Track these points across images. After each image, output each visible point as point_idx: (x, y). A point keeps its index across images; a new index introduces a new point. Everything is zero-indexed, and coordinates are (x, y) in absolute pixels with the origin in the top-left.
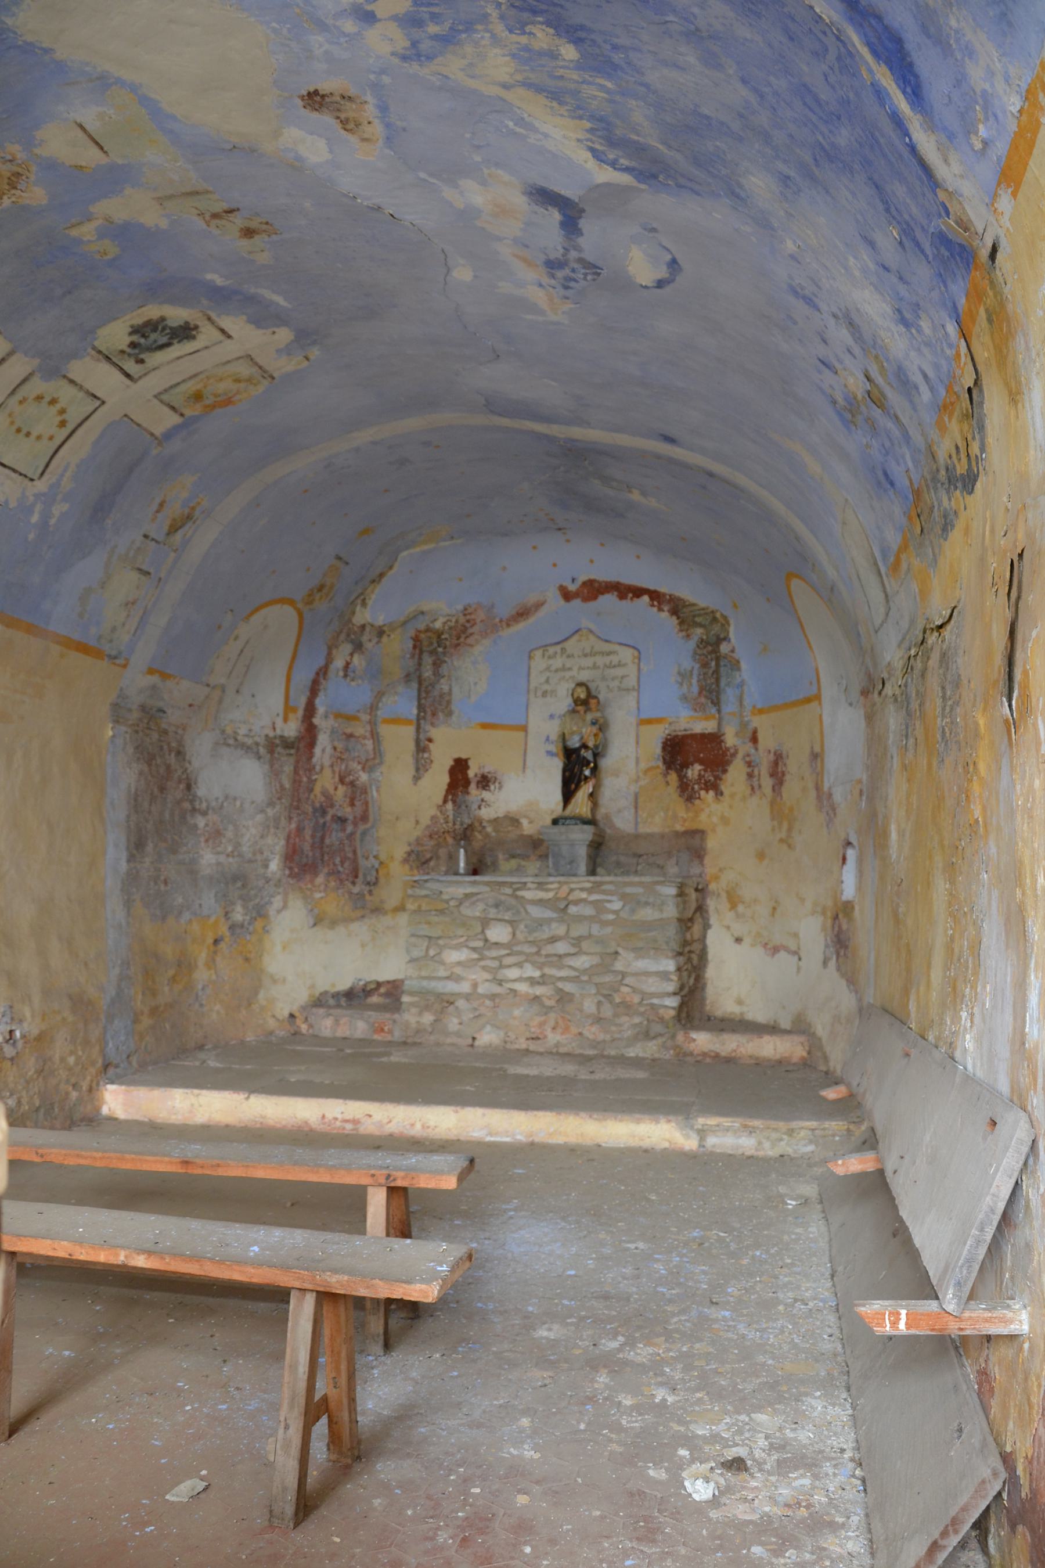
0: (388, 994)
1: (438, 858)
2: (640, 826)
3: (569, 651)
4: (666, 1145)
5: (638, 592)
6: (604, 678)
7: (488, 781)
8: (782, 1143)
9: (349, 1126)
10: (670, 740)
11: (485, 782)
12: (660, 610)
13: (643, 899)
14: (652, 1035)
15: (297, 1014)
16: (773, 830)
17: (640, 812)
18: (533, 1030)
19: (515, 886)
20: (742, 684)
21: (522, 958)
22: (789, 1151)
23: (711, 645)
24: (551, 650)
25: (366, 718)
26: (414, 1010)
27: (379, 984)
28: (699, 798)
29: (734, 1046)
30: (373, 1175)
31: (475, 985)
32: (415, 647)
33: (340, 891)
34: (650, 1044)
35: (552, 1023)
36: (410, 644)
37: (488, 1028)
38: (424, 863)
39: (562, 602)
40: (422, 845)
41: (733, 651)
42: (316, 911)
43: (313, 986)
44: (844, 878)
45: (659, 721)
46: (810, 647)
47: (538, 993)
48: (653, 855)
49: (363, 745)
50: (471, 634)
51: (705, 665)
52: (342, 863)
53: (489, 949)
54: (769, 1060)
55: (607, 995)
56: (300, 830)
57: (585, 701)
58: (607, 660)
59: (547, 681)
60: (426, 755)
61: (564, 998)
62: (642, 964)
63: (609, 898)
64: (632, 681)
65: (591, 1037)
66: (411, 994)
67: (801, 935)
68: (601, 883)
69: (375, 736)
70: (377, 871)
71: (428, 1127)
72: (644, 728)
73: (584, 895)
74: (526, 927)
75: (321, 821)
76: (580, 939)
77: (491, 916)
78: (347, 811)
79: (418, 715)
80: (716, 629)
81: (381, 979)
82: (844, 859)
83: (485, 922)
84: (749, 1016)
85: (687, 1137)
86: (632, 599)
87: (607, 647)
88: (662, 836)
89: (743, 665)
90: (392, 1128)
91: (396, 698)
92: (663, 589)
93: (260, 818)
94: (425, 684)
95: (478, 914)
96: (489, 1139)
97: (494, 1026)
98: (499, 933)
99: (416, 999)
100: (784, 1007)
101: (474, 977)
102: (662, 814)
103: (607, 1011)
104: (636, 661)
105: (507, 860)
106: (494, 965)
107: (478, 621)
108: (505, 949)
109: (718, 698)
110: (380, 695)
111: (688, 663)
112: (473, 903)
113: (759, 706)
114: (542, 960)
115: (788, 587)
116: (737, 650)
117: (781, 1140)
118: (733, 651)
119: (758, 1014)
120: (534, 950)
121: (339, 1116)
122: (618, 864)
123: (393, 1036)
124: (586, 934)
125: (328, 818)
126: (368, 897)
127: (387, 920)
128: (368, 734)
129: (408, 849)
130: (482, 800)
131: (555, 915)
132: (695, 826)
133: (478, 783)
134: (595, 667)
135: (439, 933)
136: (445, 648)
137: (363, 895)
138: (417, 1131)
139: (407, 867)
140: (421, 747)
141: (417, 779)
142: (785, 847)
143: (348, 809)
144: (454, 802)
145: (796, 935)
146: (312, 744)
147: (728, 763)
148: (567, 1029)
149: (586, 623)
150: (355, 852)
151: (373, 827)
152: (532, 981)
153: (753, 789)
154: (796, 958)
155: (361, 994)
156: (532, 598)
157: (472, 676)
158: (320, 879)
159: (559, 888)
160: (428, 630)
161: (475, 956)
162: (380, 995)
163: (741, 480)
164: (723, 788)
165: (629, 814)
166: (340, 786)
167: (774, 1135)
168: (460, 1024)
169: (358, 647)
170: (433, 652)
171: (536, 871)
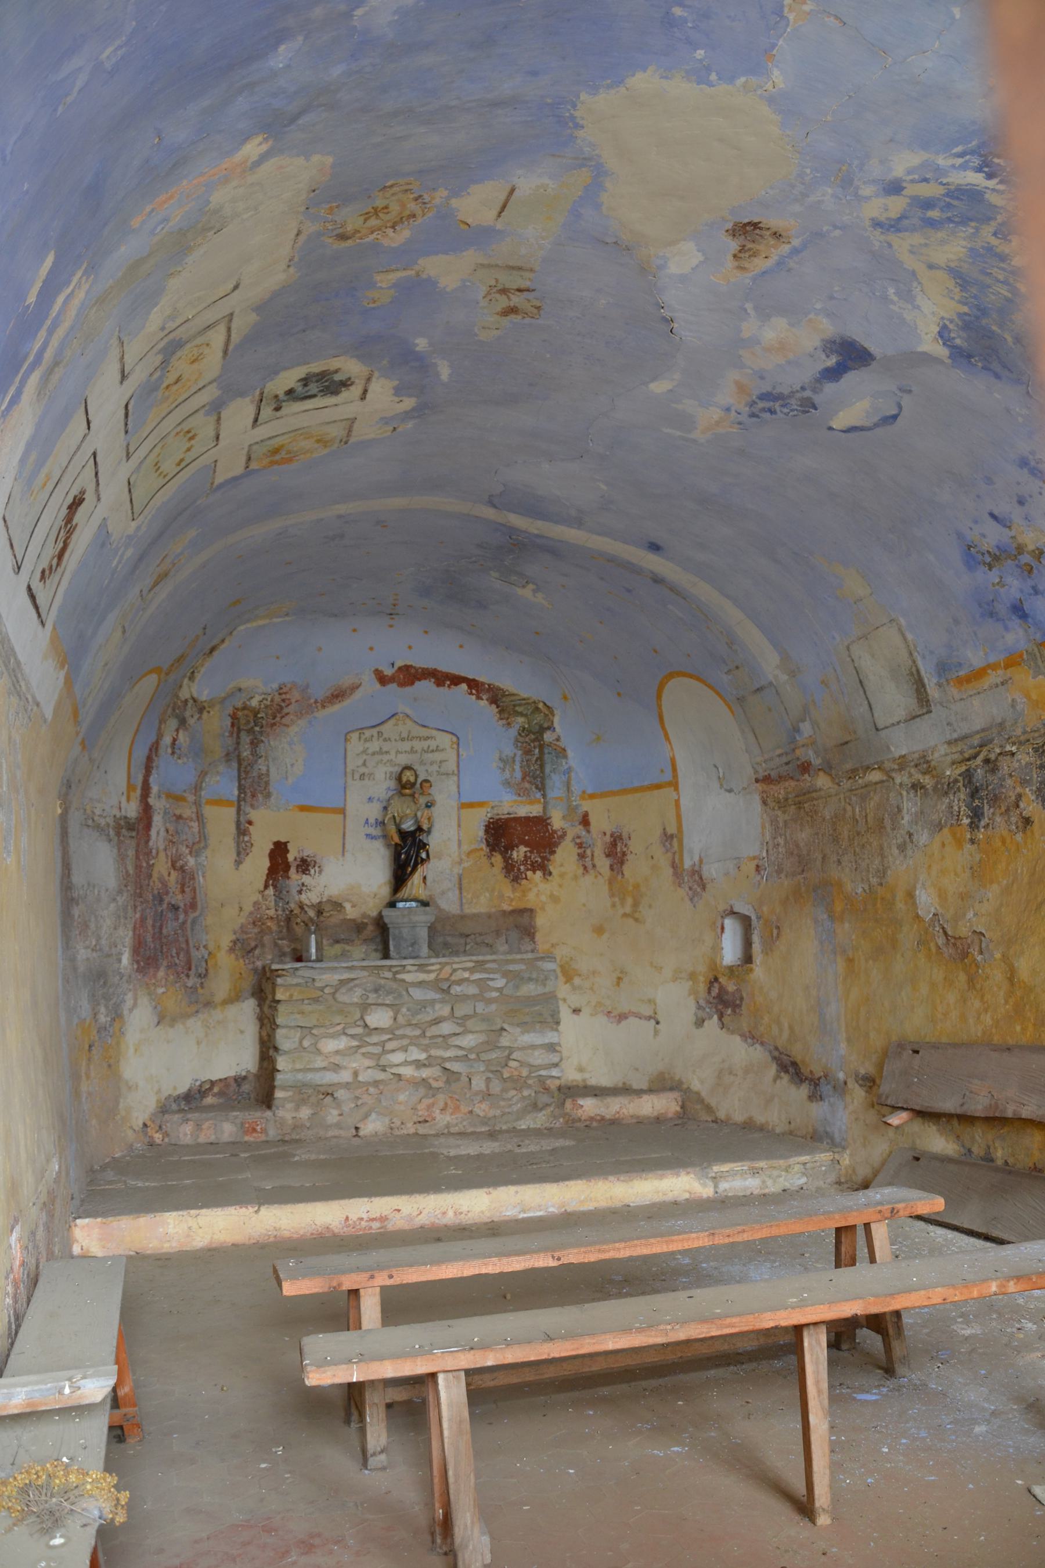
0: (221, 1094)
1: (263, 946)
2: (466, 906)
3: (385, 736)
4: (687, 1196)
5: (456, 680)
6: (422, 763)
7: (308, 865)
8: (781, 1179)
9: (376, 1225)
10: (493, 823)
11: (305, 865)
12: (479, 698)
13: (526, 975)
14: (540, 1105)
15: (149, 1123)
16: (614, 905)
17: (464, 894)
18: (420, 1113)
19: (394, 970)
20: (569, 770)
21: (405, 1042)
22: (787, 1185)
23: (534, 734)
24: (368, 733)
25: (191, 798)
26: (289, 1106)
27: (213, 1083)
28: (526, 878)
29: (617, 1108)
30: (880, 1212)
31: (356, 1074)
32: (233, 725)
33: (177, 985)
34: (540, 1115)
35: (441, 1104)
36: (228, 722)
37: (374, 1116)
38: (249, 952)
39: (378, 686)
40: (246, 933)
41: (558, 740)
42: (159, 1008)
43: (159, 1091)
44: (724, 945)
45: (481, 804)
46: (667, 738)
47: (424, 1076)
48: (481, 935)
49: (190, 827)
50: (287, 714)
51: (528, 752)
52: (178, 954)
53: (369, 1035)
54: (649, 1118)
55: (496, 1071)
56: (143, 919)
57: (408, 785)
58: (425, 744)
59: (364, 764)
60: (246, 838)
61: (451, 1076)
62: (528, 1038)
63: (491, 976)
64: (451, 766)
65: (482, 1114)
66: (284, 1088)
67: (658, 1001)
68: (484, 962)
69: (200, 818)
70: (206, 961)
71: (461, 1213)
72: (465, 812)
73: (466, 975)
74: (408, 1010)
75: (160, 909)
76: (467, 1017)
77: (370, 1001)
78: (178, 899)
79: (239, 796)
80: (538, 718)
81: (214, 1079)
82: (723, 928)
83: (365, 1007)
84: (593, 1082)
85: (704, 1185)
86: (449, 686)
87: (424, 732)
88: (489, 916)
89: (570, 753)
90: (423, 1220)
91: (218, 778)
92: (481, 679)
93: (113, 905)
94: (245, 764)
95: (356, 1000)
96: (522, 1216)
97: (379, 1114)
98: (379, 1018)
99: (290, 1093)
100: (637, 1069)
101: (354, 1065)
102: (487, 895)
103: (496, 1087)
104: (455, 746)
105: (331, 945)
106: (376, 1052)
107: (293, 701)
108: (386, 1034)
109: (543, 784)
110: (203, 774)
111: (509, 750)
112: (351, 989)
113: (590, 791)
114: (426, 1041)
115: (151, 672)
116: (562, 739)
117: (780, 1176)
118: (558, 740)
119: (601, 1078)
120: (418, 1032)
121: (365, 1216)
122: (446, 945)
123: (267, 1135)
124: (471, 1012)
125: (165, 906)
126: (200, 991)
127: (217, 1014)
128: (194, 816)
129: (234, 937)
130: (303, 884)
131: (438, 996)
132: (522, 905)
133: (298, 866)
134: (412, 751)
135: (315, 1022)
136: (262, 727)
137: (196, 988)
138: (450, 1218)
139: (233, 956)
140: (242, 830)
141: (238, 863)
142: (631, 921)
143: (180, 897)
144: (275, 887)
145: (651, 1001)
146: (148, 826)
147: (557, 844)
148: (457, 1108)
149: (401, 708)
150: (187, 942)
151: (201, 915)
152: (418, 1064)
153: (585, 868)
154: (653, 1022)
155: (197, 1096)
156: (347, 681)
157: (289, 755)
158: (161, 973)
159: (441, 970)
160: (245, 708)
161: (355, 1043)
162: (214, 1095)
163: (703, 591)
164: (551, 868)
165: (453, 895)
166: (172, 872)
167: (775, 1173)
168: (341, 1115)
169: (183, 722)
170: (250, 731)
171: (363, 956)
